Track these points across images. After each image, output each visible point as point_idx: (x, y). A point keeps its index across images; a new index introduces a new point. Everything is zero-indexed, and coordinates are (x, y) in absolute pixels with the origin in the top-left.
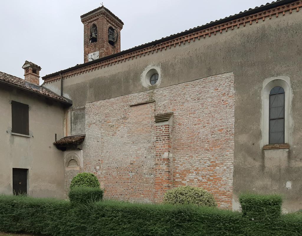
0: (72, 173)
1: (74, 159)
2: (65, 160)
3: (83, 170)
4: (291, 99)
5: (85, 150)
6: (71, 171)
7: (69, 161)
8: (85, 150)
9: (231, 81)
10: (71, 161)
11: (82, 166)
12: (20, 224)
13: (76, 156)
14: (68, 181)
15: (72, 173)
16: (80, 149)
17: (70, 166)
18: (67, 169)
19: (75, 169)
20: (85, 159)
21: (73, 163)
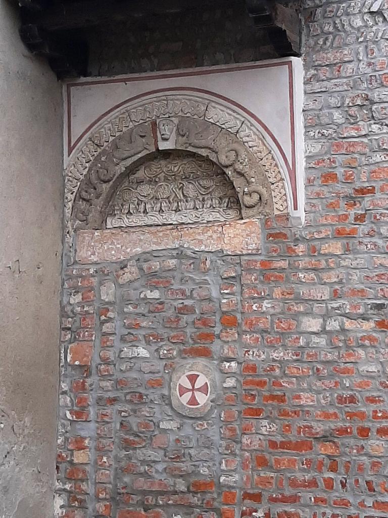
0: (153, 279)
1: (201, 143)
2: (75, 165)
3: (313, 251)
4: (172, 71)
5: (331, 56)
6: (156, 265)
7: (121, 168)
8: (331, 56)
9: (352, 399)
10: (141, 174)
11: (301, 213)
12: (295, 382)
13: (218, 114)
14: (106, 361)
15: (153, 279)
16: (280, 47)
17: (126, 222)
18: (98, 248)
19: (206, 242)
20: (337, 143)
21: (166, 190)
